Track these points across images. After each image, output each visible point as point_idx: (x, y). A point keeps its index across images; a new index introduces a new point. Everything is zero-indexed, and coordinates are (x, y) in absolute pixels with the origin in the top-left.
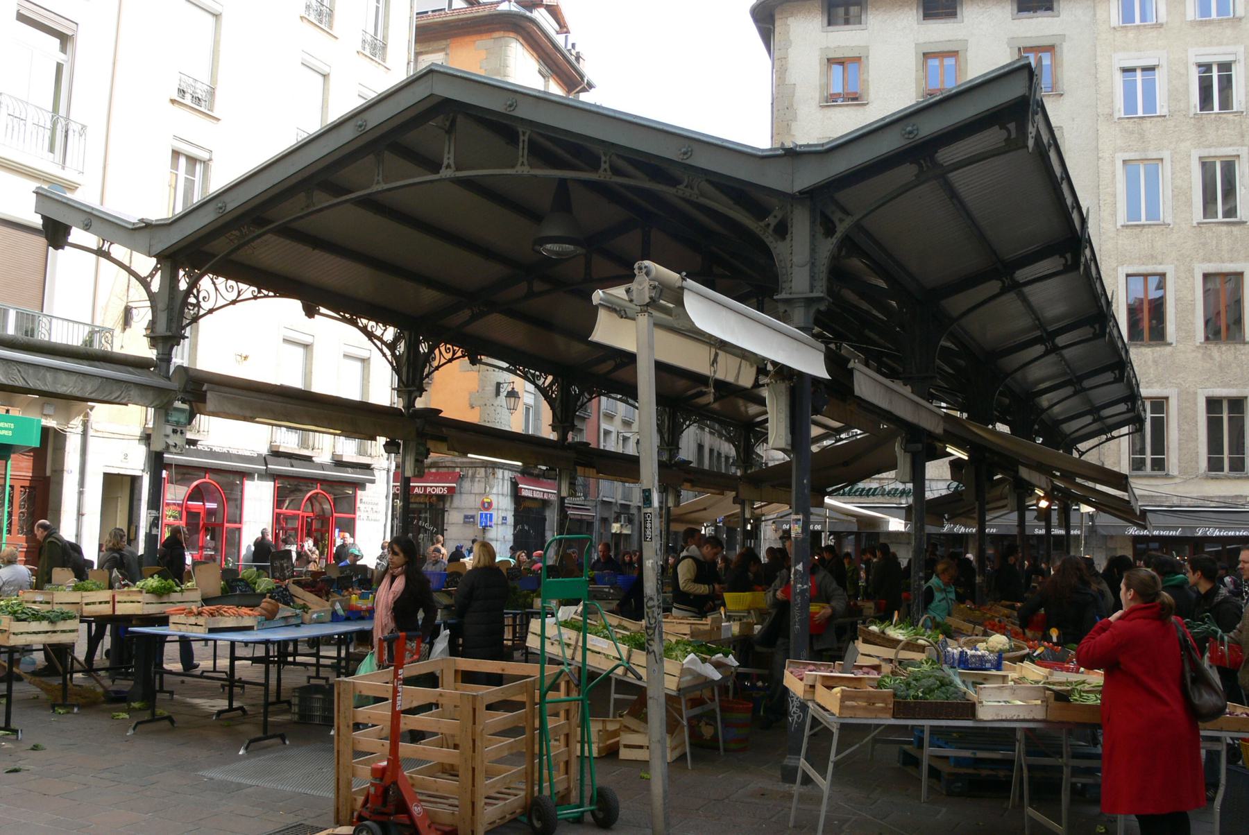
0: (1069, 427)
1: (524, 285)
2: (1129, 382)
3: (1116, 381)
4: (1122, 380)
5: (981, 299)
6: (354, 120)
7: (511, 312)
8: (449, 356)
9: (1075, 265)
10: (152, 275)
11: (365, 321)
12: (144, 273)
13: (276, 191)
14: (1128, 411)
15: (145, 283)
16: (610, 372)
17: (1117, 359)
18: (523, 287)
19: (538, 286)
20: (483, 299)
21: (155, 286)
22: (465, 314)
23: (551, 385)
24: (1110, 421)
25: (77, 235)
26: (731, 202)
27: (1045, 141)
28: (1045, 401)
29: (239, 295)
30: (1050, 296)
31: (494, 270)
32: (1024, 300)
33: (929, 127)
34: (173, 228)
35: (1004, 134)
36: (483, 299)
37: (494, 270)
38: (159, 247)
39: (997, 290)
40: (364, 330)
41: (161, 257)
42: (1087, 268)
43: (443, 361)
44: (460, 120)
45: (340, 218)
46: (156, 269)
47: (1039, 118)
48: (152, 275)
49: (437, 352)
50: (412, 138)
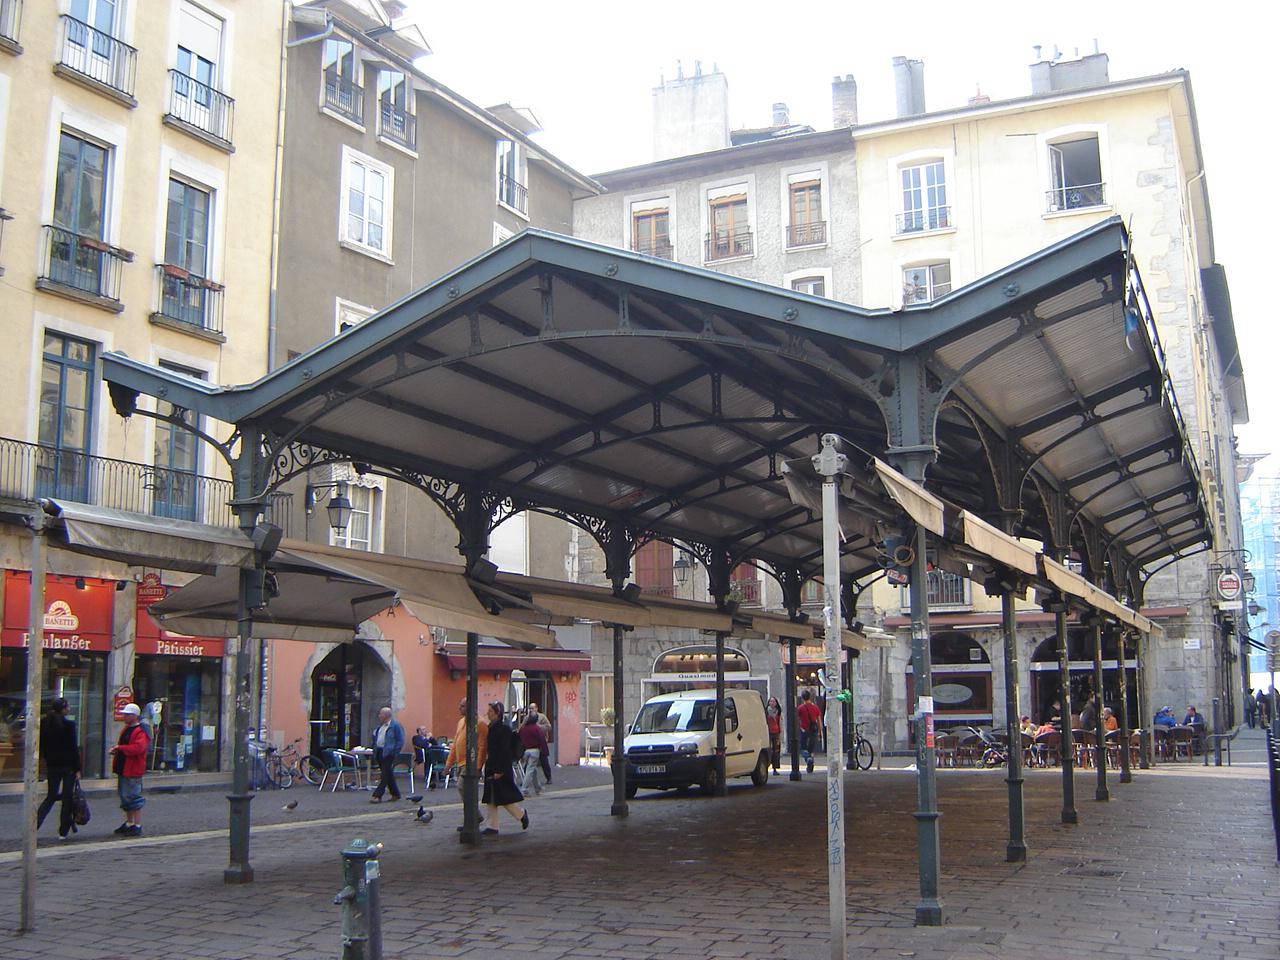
0: (1134, 549)
1: (717, 482)
2: (1187, 463)
3: (1171, 461)
4: (1211, 548)
5: (1103, 495)
6: (446, 287)
7: (573, 461)
8: (304, 461)
9: (1178, 458)
10: (231, 442)
11: (428, 479)
12: (222, 440)
13: (360, 357)
14: (1197, 527)
15: (224, 449)
16: (320, 414)
17: (1147, 368)
18: (715, 484)
19: (605, 436)
20: (545, 452)
21: (236, 452)
22: (530, 467)
23: (457, 496)
24: (1176, 540)
25: (146, 401)
26: (827, 356)
27: (1144, 316)
28: (1081, 492)
29: (312, 459)
30: (1126, 428)
31: (562, 422)
32: (1048, 348)
33: (1028, 286)
34: (258, 393)
35: (1101, 286)
36: (545, 452)
37: (562, 422)
38: (241, 414)
39: (1079, 425)
40: (427, 490)
41: (241, 425)
42: (1134, 301)
43: (504, 515)
44: (559, 285)
45: (435, 385)
46: (235, 436)
47: (1132, 272)
48: (231, 442)
49: (498, 508)
50: (506, 300)
